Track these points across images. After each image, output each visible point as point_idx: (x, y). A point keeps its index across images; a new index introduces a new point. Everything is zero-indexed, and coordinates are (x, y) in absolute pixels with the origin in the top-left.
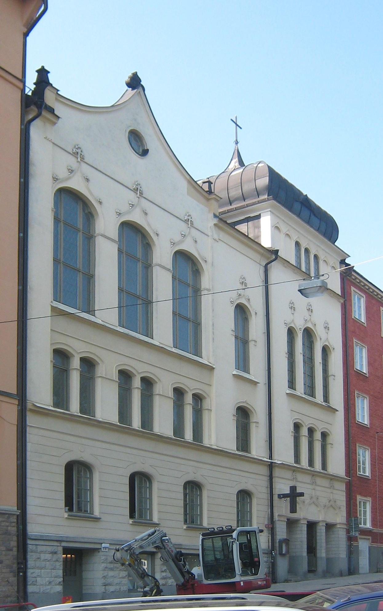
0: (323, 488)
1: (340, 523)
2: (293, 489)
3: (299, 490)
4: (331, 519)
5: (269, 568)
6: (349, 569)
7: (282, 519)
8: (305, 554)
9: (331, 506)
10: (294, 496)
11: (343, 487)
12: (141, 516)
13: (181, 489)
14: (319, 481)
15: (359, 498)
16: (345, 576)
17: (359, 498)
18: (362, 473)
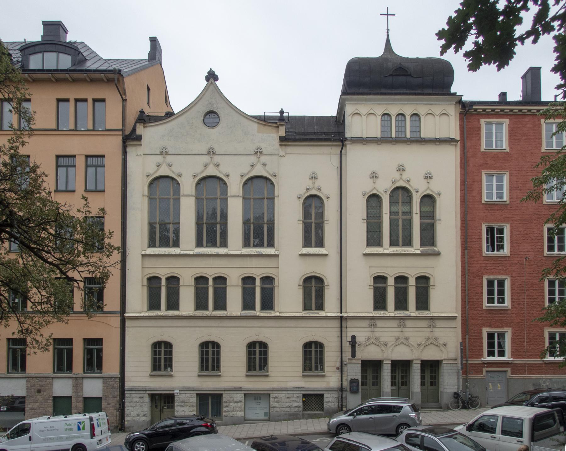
13: (301, 349)
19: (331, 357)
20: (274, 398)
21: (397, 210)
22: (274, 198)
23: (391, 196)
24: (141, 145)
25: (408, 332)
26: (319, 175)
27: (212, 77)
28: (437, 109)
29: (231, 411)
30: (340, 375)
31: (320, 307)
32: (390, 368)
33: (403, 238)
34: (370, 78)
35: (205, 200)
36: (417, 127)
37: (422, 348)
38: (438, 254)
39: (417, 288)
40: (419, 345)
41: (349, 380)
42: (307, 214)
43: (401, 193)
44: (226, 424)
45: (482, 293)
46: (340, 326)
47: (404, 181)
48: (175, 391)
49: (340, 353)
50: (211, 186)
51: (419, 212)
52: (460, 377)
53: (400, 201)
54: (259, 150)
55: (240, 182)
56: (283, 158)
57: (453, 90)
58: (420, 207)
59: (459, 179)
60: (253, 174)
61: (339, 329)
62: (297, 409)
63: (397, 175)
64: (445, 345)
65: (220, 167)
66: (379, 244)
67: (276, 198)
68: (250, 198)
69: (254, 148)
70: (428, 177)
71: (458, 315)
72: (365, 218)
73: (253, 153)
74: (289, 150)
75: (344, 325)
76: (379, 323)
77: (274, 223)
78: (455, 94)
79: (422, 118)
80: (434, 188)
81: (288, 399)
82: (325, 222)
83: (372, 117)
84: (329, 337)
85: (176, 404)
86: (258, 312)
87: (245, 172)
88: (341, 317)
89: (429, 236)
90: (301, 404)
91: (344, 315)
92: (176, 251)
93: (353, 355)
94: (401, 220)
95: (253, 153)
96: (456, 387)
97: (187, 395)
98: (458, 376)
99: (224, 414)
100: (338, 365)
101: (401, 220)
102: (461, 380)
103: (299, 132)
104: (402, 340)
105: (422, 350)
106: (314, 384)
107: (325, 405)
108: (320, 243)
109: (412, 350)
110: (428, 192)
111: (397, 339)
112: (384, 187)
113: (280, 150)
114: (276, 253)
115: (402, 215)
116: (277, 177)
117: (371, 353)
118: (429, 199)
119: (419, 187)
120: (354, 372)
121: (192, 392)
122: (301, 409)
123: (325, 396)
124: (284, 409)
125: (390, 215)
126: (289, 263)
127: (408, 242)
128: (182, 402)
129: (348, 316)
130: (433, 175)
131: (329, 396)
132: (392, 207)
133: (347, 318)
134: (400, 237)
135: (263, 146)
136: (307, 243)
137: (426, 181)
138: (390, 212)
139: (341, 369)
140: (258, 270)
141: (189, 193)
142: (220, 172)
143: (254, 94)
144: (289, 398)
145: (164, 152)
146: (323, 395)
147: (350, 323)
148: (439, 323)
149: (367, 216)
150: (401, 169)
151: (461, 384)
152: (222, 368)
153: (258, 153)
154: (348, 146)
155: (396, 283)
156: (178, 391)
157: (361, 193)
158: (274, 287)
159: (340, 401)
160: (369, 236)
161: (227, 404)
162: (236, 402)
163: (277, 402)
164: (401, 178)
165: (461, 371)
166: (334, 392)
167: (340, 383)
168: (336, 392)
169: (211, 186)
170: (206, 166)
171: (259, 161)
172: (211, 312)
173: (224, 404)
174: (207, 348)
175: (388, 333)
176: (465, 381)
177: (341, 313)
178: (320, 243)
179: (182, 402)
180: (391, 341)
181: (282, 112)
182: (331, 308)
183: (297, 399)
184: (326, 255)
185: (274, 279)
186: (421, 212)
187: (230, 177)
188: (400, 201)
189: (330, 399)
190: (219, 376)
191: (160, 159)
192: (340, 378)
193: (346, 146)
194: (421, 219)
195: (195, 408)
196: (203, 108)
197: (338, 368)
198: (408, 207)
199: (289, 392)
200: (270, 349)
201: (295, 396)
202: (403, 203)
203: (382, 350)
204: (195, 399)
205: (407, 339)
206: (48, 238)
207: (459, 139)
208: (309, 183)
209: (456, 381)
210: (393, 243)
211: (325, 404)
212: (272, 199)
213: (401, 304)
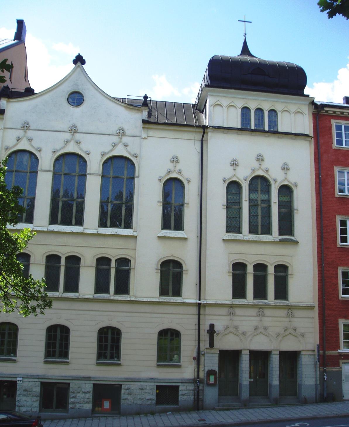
13: (44, 333)
19: (188, 346)
20: (126, 389)
21: (256, 198)
22: (133, 179)
23: (250, 184)
24: (3, 118)
25: (267, 321)
26: (180, 159)
27: (79, 60)
28: (293, 108)
29: (79, 403)
30: (196, 366)
31: (178, 292)
33: (262, 226)
34: (225, 74)
35: (63, 176)
36: (273, 122)
37: (280, 338)
38: (296, 243)
39: (276, 277)
40: (278, 335)
42: (166, 195)
43: (260, 183)
44: (73, 418)
45: (338, 283)
46: (197, 313)
47: (263, 170)
48: (18, 379)
49: (197, 342)
50: (70, 165)
51: (277, 201)
52: (318, 369)
53: (259, 189)
54: (26, 124)
55: (101, 161)
56: (145, 140)
57: (306, 91)
58: (278, 196)
59: (314, 173)
60: (20, 147)
61: (197, 316)
62: (150, 401)
63: (256, 165)
64: (303, 335)
65: (81, 145)
66: (239, 230)
67: (136, 179)
68: (75, 175)
69: (117, 129)
70: (286, 168)
71: (316, 304)
72: (225, 204)
73: (19, 127)
74: (151, 133)
75: (202, 312)
76: (238, 311)
77: (84, 201)
78: (308, 96)
79: (279, 114)
80: (291, 179)
81: (141, 391)
82: (185, 205)
83: (232, 109)
84: (184, 323)
85: (18, 393)
86: (112, 295)
87: (106, 151)
88: (200, 304)
89: (287, 226)
90: (154, 397)
91: (203, 302)
92: (77, 229)
93: (212, 344)
94: (260, 208)
95: (68, 131)
96: (314, 379)
97: (31, 383)
98: (316, 368)
99: (70, 406)
100: (195, 355)
101: (260, 208)
102: (318, 373)
103: (155, 115)
104: (231, 329)
105: (281, 341)
106: (169, 375)
107: (180, 398)
108: (179, 226)
109: (270, 340)
110: (286, 183)
111: (256, 328)
112: (243, 175)
113: (143, 132)
114: (186, 236)
115: (261, 203)
116: (138, 158)
117: (227, 342)
118: (286, 190)
119: (277, 179)
120: (212, 362)
121: (37, 380)
122: (154, 402)
123: (180, 388)
124: (135, 402)
125: (249, 203)
126: (147, 243)
127: (267, 231)
128: (25, 391)
129: (207, 303)
130: (291, 166)
131: (184, 388)
132: (251, 195)
133: (205, 305)
134: (261, 226)
135: (126, 127)
136: (166, 226)
137: (232, 168)
138: (250, 199)
139: (198, 359)
140: (114, 251)
141: (47, 168)
142: (81, 149)
143: (117, 78)
144: (142, 389)
145: (26, 127)
146: (178, 387)
147: (208, 310)
148: (297, 313)
149: (227, 202)
150: (260, 159)
151: (318, 376)
152: (70, 355)
153: (121, 133)
154: (210, 134)
155: (254, 270)
156: (21, 379)
157: (222, 179)
158: (60, 266)
159: (196, 394)
160: (229, 222)
161: (74, 395)
162: (84, 393)
163: (129, 394)
164: (260, 168)
165: (318, 363)
167: (196, 374)
169: (70, 165)
170: (19, 139)
171: (120, 142)
172: (112, 295)
173: (71, 395)
174: (56, 332)
175: (247, 320)
176: (322, 373)
177: (200, 300)
178: (179, 226)
179: (25, 391)
180: (256, 330)
181: (146, 97)
182: (189, 294)
183: (150, 391)
184: (186, 239)
185: (130, 261)
186: (279, 201)
187: (41, 152)
188: (259, 189)
189: (186, 392)
190: (67, 363)
191: (20, 133)
192: (196, 370)
193: (207, 133)
194: (279, 208)
195: (39, 398)
196: (68, 88)
197: (194, 358)
198: (267, 196)
199: (142, 383)
200: (123, 335)
201: (148, 387)
202: (262, 191)
203: (241, 340)
204: (39, 387)
205: (266, 329)
206: (238, 224)
207: (313, 136)
208: (171, 166)
209: (314, 373)
210: (251, 232)
211: (180, 397)
212: (131, 179)
213: (260, 292)
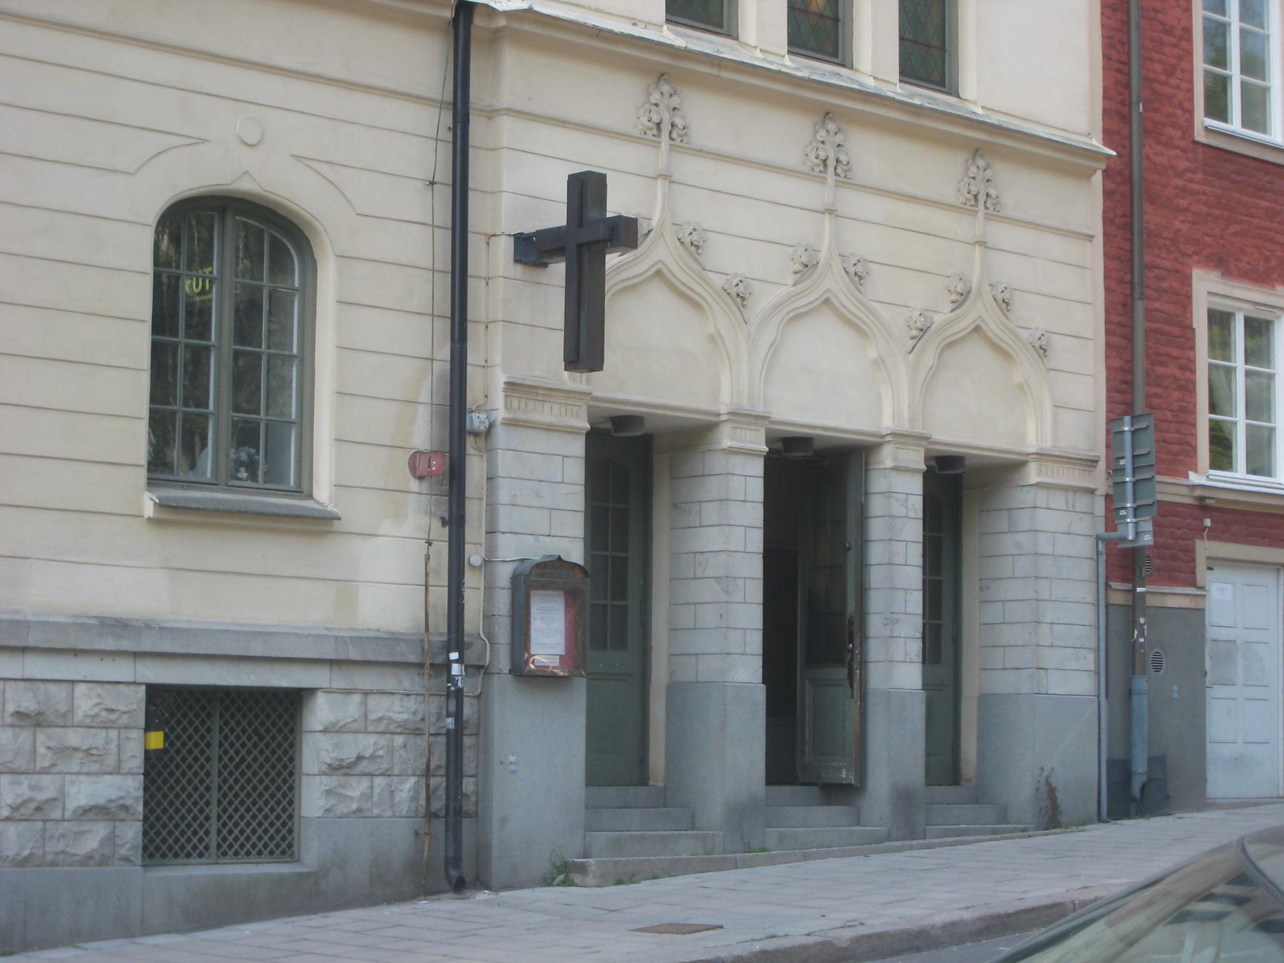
0: (905, 212)
1: (1042, 456)
2: (586, 189)
3: (617, 204)
4: (973, 420)
5: (427, 773)
6: (1119, 772)
7: (546, 414)
8: (747, 670)
9: (977, 329)
10: (585, 240)
11: (1085, 206)
12: (269, 477)
13: (137, 251)
14: (870, 153)
15: (1207, 288)
16: (1082, 823)
17: (1207, 288)
18: (1235, 125)
32: (756, 490)
41: (504, 574)
90: (130, 787)
100: (422, 432)
106: (235, 599)
131: (351, 708)
166: (387, 681)
167: (440, 594)
168: (409, 681)
183: (98, 738)
189: (367, 744)
199: (38, 667)
201: (85, 702)
203: (715, 340)
